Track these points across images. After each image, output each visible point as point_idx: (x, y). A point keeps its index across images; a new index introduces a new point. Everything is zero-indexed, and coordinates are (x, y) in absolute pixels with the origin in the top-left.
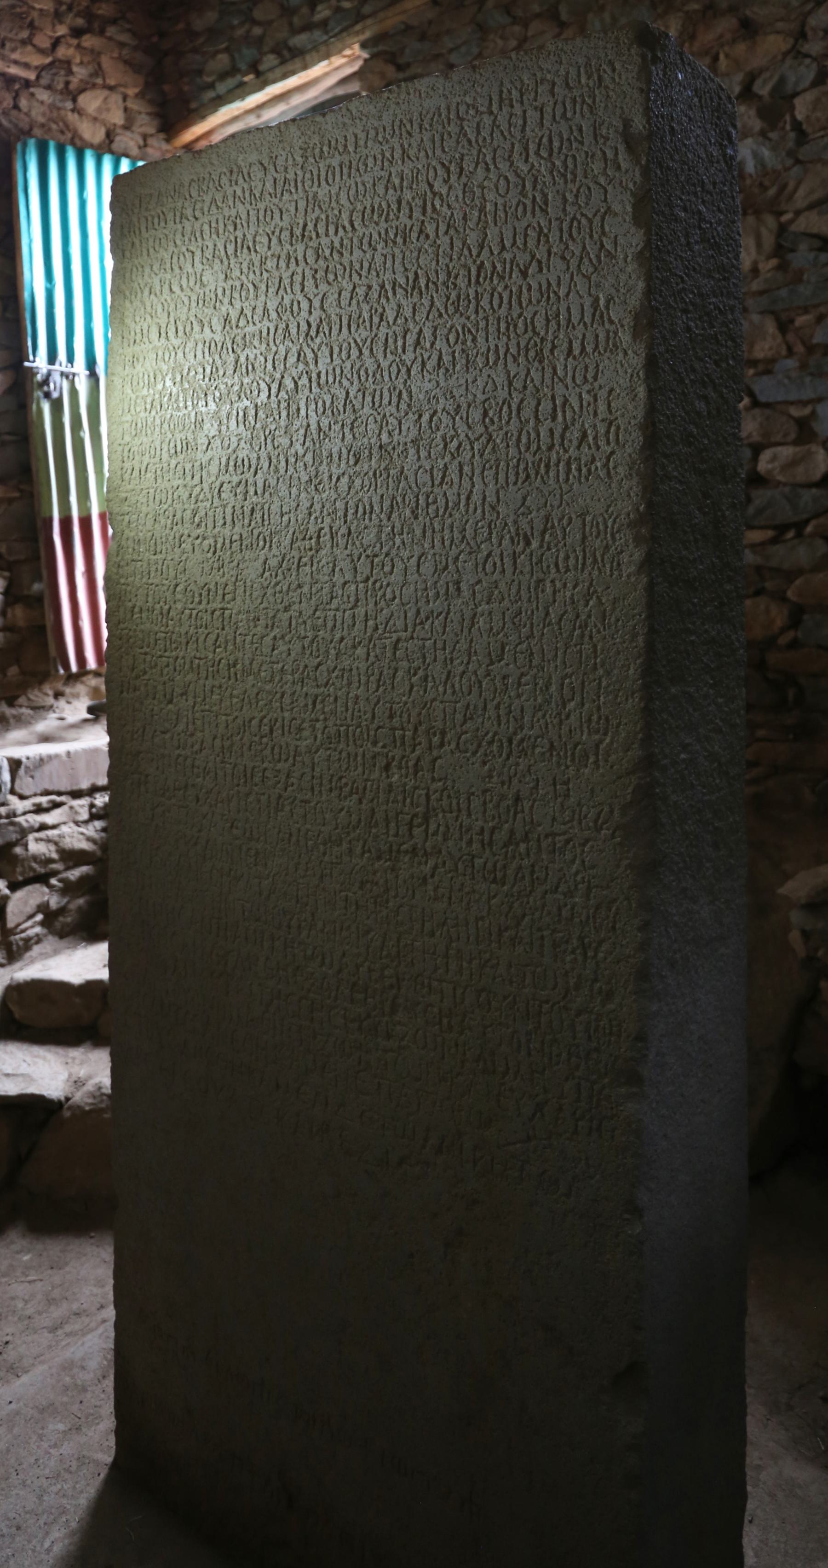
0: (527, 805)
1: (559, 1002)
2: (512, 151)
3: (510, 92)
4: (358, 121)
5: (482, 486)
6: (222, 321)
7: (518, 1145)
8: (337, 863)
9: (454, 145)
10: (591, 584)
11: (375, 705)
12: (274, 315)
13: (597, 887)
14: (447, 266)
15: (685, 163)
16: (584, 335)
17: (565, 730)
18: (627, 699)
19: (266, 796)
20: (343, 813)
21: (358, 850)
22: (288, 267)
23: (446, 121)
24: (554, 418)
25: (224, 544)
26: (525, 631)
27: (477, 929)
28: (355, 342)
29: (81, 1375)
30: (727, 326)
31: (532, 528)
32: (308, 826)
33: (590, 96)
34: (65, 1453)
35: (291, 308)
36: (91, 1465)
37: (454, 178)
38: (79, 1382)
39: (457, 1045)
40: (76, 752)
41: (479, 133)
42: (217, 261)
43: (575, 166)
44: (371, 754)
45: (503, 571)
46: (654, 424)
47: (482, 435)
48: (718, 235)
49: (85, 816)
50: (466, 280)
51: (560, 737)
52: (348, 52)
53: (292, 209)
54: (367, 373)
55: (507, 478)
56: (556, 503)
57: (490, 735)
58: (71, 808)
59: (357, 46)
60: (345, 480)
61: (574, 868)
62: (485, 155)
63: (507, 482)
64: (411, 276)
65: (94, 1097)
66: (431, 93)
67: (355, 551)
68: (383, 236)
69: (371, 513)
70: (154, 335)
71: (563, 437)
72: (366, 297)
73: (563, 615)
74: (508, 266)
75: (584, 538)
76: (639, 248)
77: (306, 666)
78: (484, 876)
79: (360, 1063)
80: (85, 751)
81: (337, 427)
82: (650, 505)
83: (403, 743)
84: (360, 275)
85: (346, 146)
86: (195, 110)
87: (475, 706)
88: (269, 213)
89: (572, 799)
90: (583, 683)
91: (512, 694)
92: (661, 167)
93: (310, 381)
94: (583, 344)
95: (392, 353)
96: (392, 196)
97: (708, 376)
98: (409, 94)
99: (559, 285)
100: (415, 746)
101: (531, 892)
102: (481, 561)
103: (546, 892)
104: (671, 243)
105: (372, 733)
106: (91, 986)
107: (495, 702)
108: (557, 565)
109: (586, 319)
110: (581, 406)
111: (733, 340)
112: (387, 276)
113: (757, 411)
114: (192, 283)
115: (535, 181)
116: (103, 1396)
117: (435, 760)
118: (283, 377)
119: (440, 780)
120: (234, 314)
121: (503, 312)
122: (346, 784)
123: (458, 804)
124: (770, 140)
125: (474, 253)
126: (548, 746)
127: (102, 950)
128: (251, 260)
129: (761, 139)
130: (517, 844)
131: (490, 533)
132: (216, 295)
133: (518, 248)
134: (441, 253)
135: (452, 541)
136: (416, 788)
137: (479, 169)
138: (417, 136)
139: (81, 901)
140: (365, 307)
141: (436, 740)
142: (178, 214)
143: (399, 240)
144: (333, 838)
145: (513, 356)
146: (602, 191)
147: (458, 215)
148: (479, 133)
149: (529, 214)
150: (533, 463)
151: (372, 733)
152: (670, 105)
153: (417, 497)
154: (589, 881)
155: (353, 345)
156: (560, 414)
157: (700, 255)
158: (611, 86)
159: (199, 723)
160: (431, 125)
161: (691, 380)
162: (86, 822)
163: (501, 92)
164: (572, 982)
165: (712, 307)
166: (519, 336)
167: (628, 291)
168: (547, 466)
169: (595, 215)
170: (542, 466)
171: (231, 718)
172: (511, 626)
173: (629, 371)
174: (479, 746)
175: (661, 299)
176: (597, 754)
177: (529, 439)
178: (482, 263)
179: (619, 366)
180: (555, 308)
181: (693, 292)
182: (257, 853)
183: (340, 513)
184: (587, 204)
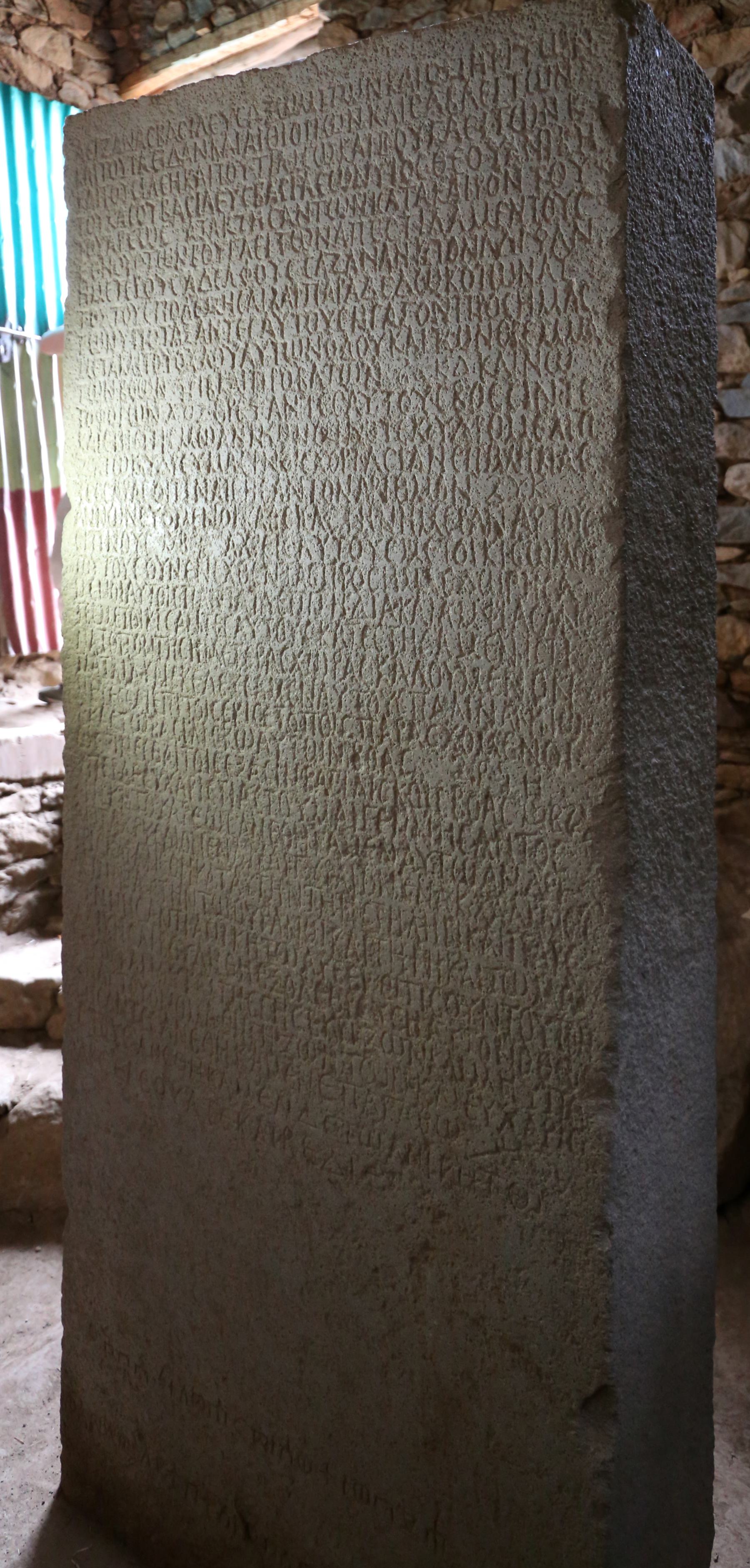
0: (497, 803)
1: (528, 1008)
2: (484, 121)
3: (481, 56)
4: (323, 77)
5: (452, 472)
6: (184, 282)
7: (487, 1156)
8: (302, 856)
9: (423, 110)
10: (563, 578)
11: (342, 693)
12: (237, 280)
13: (568, 890)
14: (417, 239)
15: (661, 147)
16: (557, 321)
17: (535, 728)
18: (599, 698)
19: (229, 783)
20: (308, 804)
21: (323, 844)
22: (252, 230)
23: (415, 84)
24: (526, 405)
25: (186, 519)
26: (495, 623)
27: (446, 929)
28: (322, 313)
29: (24, 1398)
30: (701, 324)
31: (503, 517)
32: (273, 816)
33: (564, 68)
34: (6, 1480)
35: (256, 273)
36: (35, 1493)
37: (423, 145)
38: (23, 1405)
39: (424, 1050)
40: (27, 739)
41: (449, 99)
42: (178, 218)
43: (549, 142)
44: (338, 744)
45: (473, 561)
46: (627, 417)
47: (451, 419)
48: (693, 227)
49: (36, 806)
50: (436, 255)
51: (531, 733)
52: (306, 12)
53: (256, 167)
54: (334, 347)
55: (478, 464)
56: (527, 493)
57: (460, 728)
58: (21, 797)
59: (316, 7)
60: (311, 458)
61: (545, 869)
62: (455, 124)
63: (477, 469)
64: (379, 247)
65: (42, 1102)
66: (400, 52)
67: (322, 531)
68: (351, 203)
69: (338, 493)
70: (113, 295)
71: (535, 425)
72: (333, 266)
73: (534, 609)
74: (479, 243)
75: (556, 530)
76: (614, 233)
77: (271, 649)
78: (452, 875)
79: (323, 1067)
80: (37, 738)
81: (304, 403)
82: (623, 499)
83: (370, 734)
84: (327, 244)
85: (311, 103)
86: (146, 63)
87: (445, 699)
88: (231, 170)
89: (543, 799)
90: (554, 679)
91: (482, 687)
92: (637, 149)
93: (276, 351)
94: (555, 330)
95: (359, 327)
96: (360, 164)
97: (681, 373)
98: (376, 51)
99: (531, 266)
100: (383, 737)
101: (500, 893)
102: (450, 549)
103: (516, 893)
104: (646, 231)
105: (339, 721)
106: (40, 987)
107: (465, 695)
108: (528, 557)
109: (559, 304)
110: (554, 394)
111: (707, 340)
112: (355, 246)
113: (725, 426)
114: (151, 240)
115: (508, 156)
116: (47, 1419)
117: (403, 752)
118: (247, 345)
119: (409, 773)
120: (196, 276)
121: (474, 292)
122: (312, 774)
123: (427, 799)
124: (742, 142)
125: (445, 228)
126: (518, 743)
127: (55, 946)
128: (213, 219)
129: (733, 141)
130: (487, 843)
131: (461, 520)
132: (177, 255)
133: (489, 225)
134: (410, 226)
135: (421, 526)
136: (384, 780)
137: (449, 139)
138: (385, 99)
139: (30, 896)
140: (332, 277)
141: (404, 731)
142: (136, 164)
143: (368, 209)
144: (298, 830)
145: (484, 338)
146: (576, 170)
147: (428, 187)
148: (449, 99)
149: (500, 189)
150: (504, 451)
151: (339, 721)
152: (647, 83)
153: (386, 479)
154: (560, 884)
155: (320, 317)
156: (532, 401)
157: (675, 247)
158: (588, 58)
159: (159, 704)
160: (399, 87)
161: (665, 376)
162: (37, 813)
163: (473, 56)
164: (542, 987)
165: (686, 302)
166: (490, 317)
167: (602, 277)
168: (519, 454)
169: (569, 195)
170: (514, 453)
171: (192, 701)
172: (482, 617)
173: (603, 361)
174: (449, 739)
175: (635, 289)
176: (568, 753)
177: (500, 425)
178: (453, 238)
179: (592, 354)
180: (527, 291)
181: (667, 285)
182: (219, 844)
183: (307, 492)
184: (561, 183)
